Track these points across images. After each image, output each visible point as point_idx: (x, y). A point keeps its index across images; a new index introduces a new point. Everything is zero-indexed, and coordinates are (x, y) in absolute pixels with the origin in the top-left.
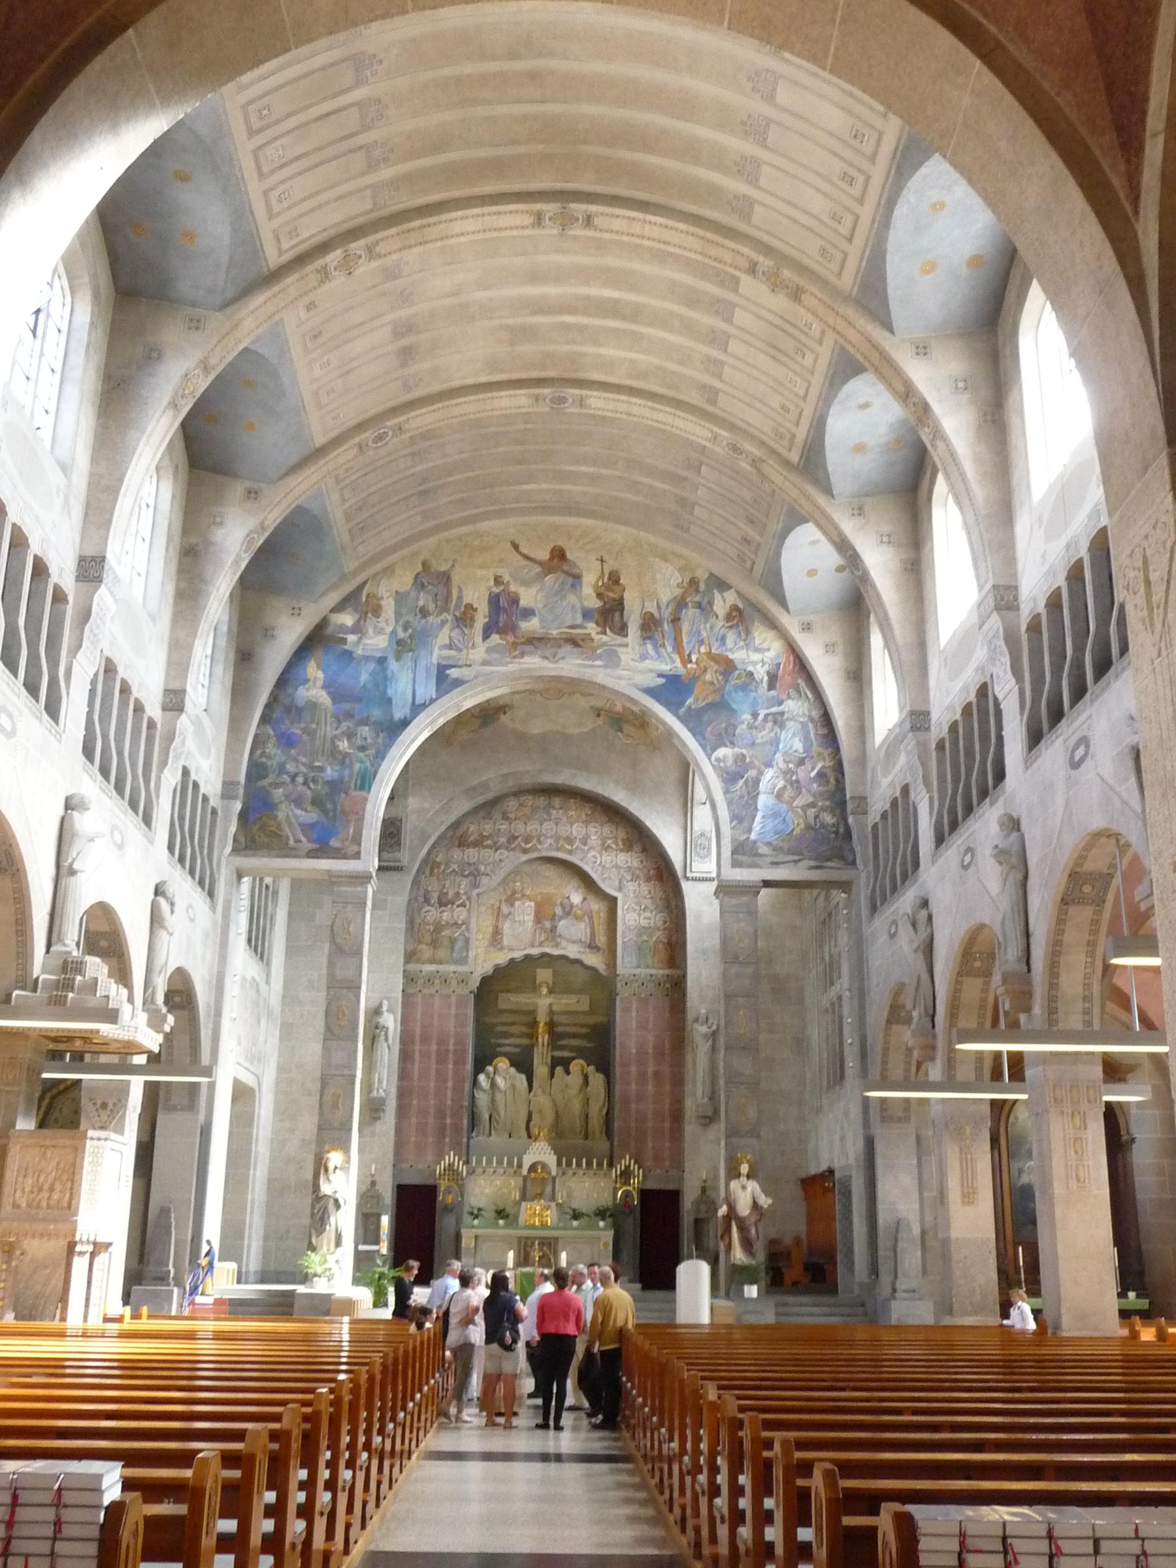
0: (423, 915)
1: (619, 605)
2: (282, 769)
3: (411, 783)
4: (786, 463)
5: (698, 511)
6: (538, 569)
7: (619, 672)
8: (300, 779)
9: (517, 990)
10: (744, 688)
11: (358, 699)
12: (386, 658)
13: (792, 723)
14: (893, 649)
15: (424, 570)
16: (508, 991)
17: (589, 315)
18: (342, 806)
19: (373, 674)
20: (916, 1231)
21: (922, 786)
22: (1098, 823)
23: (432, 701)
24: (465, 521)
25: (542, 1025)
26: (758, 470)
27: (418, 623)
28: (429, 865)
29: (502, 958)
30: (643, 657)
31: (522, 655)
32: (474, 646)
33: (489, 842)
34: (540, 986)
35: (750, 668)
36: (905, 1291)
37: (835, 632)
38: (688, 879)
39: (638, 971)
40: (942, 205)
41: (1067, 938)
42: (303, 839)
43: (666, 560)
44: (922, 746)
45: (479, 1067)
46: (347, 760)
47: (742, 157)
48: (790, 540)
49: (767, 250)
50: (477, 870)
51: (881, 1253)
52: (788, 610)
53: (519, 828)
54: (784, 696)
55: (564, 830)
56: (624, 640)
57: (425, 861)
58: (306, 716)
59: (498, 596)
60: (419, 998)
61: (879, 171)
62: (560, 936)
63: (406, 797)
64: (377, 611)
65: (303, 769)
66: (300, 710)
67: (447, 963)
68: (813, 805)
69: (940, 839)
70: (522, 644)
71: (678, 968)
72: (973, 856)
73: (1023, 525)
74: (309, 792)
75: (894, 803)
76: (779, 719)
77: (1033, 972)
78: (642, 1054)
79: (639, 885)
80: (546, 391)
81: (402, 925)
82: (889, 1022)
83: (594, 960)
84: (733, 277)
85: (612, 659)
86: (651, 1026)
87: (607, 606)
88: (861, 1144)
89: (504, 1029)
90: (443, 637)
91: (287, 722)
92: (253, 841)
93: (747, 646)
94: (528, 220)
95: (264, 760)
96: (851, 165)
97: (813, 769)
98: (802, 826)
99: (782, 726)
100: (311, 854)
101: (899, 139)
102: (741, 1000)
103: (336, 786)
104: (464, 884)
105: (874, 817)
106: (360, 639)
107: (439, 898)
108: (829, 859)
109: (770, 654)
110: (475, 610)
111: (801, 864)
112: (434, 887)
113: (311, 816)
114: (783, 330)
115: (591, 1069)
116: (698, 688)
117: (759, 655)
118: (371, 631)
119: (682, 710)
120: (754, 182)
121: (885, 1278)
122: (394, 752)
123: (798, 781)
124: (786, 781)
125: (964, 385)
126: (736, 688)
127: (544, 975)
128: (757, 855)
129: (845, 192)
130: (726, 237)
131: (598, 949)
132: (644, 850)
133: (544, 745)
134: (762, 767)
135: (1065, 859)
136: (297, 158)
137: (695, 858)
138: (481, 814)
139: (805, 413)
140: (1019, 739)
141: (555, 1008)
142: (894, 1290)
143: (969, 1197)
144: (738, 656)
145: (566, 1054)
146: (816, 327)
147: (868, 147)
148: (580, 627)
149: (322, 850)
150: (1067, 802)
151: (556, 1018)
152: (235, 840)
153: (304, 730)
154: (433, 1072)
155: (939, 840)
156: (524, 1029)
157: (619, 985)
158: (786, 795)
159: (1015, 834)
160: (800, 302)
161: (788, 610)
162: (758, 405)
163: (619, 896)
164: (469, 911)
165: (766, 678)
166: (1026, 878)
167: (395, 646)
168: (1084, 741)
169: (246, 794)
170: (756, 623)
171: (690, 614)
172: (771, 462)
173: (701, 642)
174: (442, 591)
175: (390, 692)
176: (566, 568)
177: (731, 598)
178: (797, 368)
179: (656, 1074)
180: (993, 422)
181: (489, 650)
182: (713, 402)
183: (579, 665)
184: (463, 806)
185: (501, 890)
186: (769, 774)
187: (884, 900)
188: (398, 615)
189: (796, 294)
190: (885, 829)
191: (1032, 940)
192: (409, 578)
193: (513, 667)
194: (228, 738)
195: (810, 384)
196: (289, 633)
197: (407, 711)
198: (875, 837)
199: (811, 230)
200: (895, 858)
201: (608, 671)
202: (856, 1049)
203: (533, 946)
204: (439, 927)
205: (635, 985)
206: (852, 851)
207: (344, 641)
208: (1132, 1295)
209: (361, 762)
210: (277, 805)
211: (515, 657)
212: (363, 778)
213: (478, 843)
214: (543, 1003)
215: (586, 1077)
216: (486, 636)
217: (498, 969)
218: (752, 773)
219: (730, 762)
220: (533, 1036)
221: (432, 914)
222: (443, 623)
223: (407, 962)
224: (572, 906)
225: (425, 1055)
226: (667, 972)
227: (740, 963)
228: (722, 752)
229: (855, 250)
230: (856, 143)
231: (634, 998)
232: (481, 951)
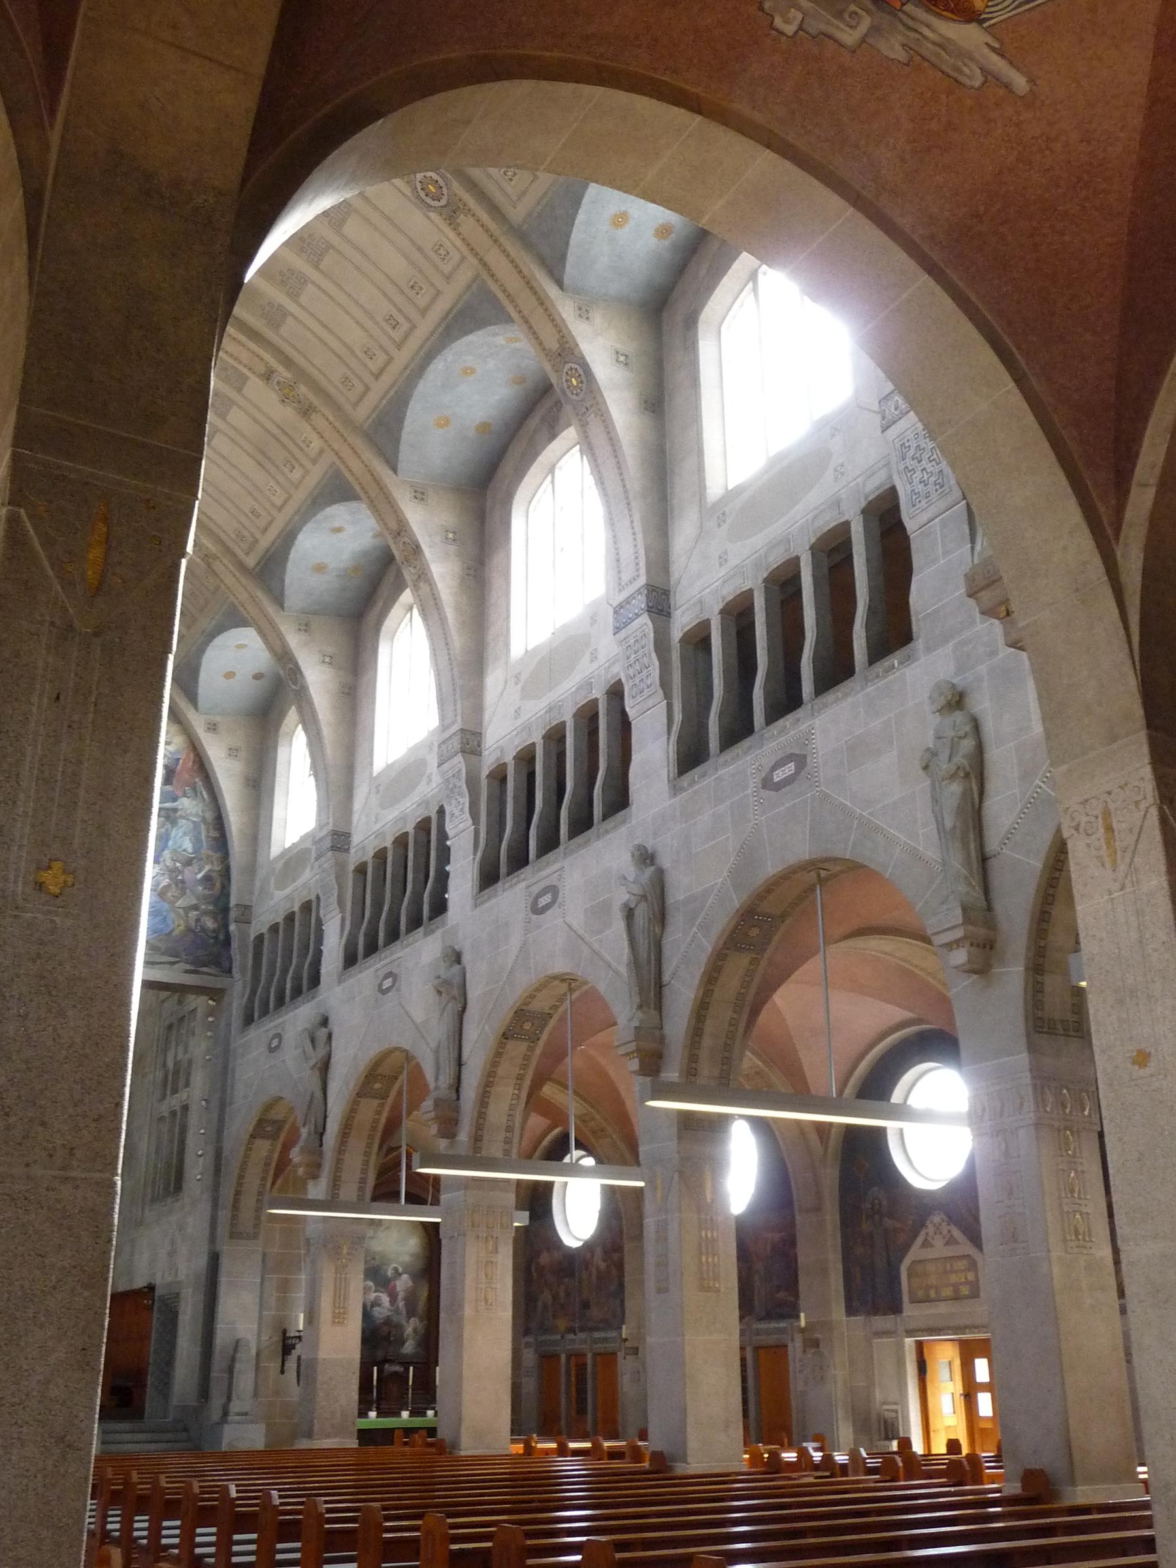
4: (242, 566)
20: (254, 1352)
21: (336, 905)
22: (561, 966)
26: (209, 565)
36: (238, 1414)
40: (473, 371)
41: (501, 1071)
44: (341, 867)
47: (289, 270)
48: (219, 641)
49: (288, 362)
51: (214, 1374)
54: (179, 793)
61: (426, 326)
68: (195, 907)
72: (394, 982)
73: (494, 680)
75: (290, 918)
76: (172, 814)
77: (462, 1101)
82: (253, 1136)
84: (242, 375)
88: (202, 1262)
96: (400, 310)
98: (182, 928)
99: (174, 823)
101: (455, 304)
105: (254, 930)
114: (278, 440)
120: (294, 296)
121: (217, 1402)
124: (171, 879)
125: (454, 537)
129: (386, 333)
130: (250, 338)
135: (512, 999)
140: (469, 876)
142: (226, 1413)
143: (339, 1317)
146: (316, 444)
147: (422, 301)
150: (525, 944)
155: (350, 960)
158: (169, 894)
159: (457, 967)
160: (308, 420)
162: (228, 504)
166: (464, 1008)
168: (553, 890)
172: (226, 561)
178: (281, 479)
180: (475, 576)
187: (265, 1012)
189: (306, 412)
190: (274, 943)
191: (464, 1070)
195: (290, 496)
199: (339, 357)
200: (285, 971)
206: (230, 959)
208: (373, 1414)
229: (378, 389)
230: (412, 294)
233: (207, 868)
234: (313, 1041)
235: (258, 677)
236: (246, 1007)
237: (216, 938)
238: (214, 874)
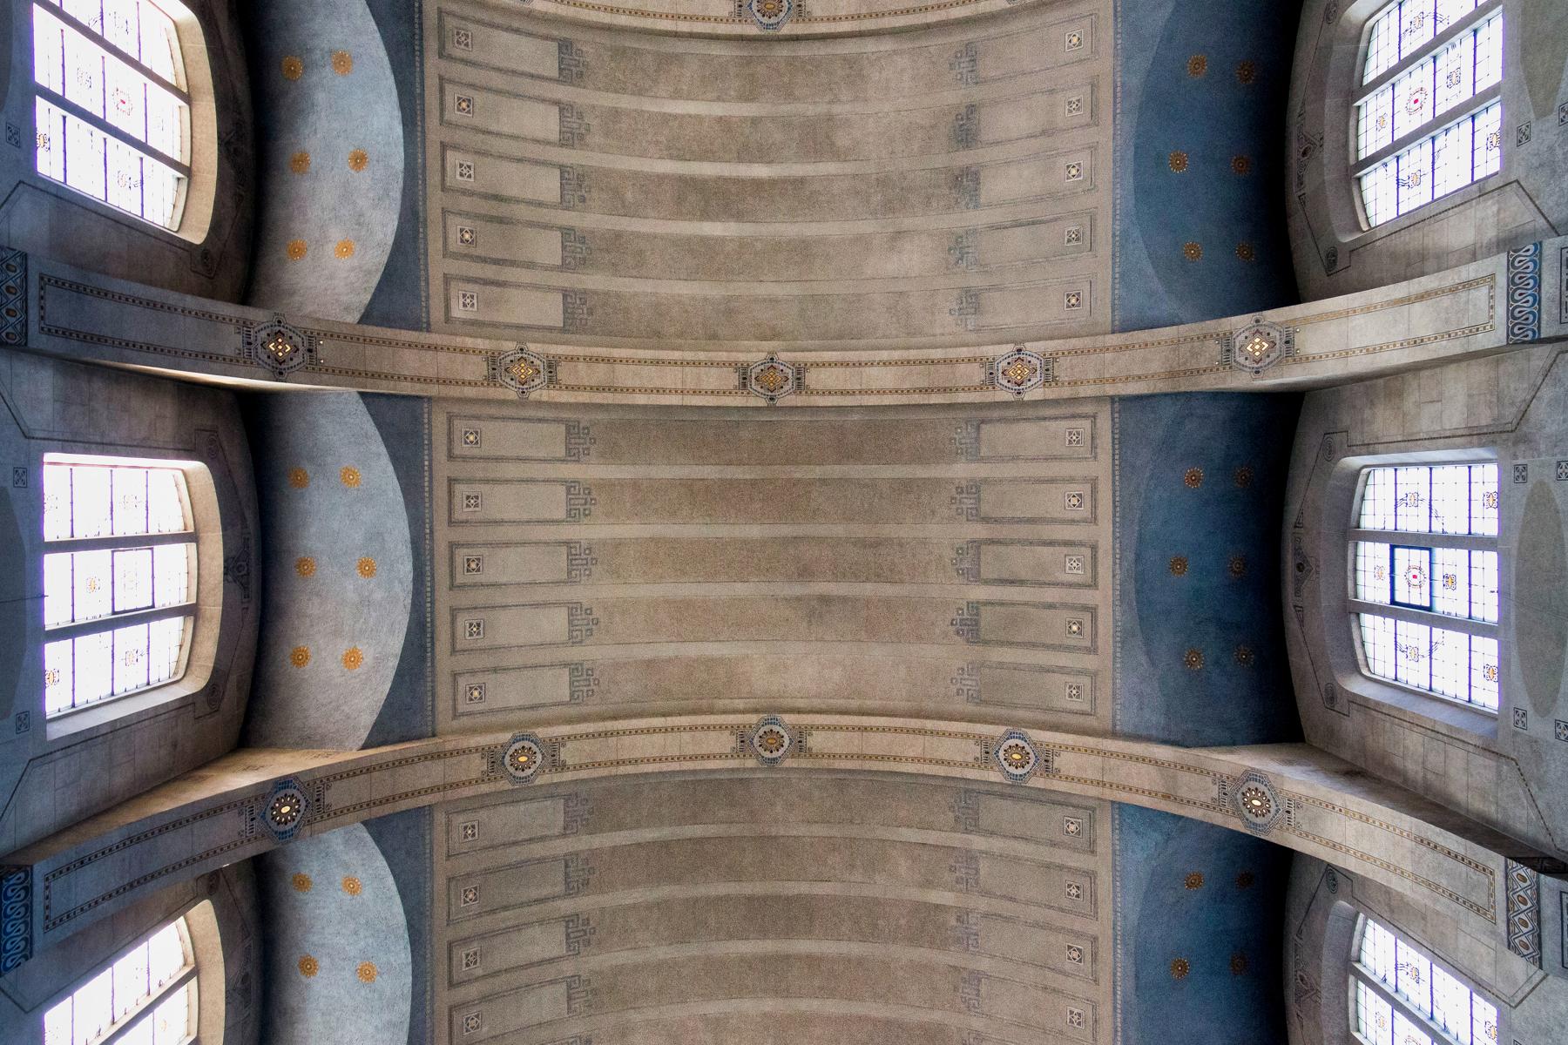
17: (737, 181)
94: (813, 378)
96: (482, 650)
101: (433, 665)
114: (496, 262)
136: (1051, 543)
182: (565, 46)
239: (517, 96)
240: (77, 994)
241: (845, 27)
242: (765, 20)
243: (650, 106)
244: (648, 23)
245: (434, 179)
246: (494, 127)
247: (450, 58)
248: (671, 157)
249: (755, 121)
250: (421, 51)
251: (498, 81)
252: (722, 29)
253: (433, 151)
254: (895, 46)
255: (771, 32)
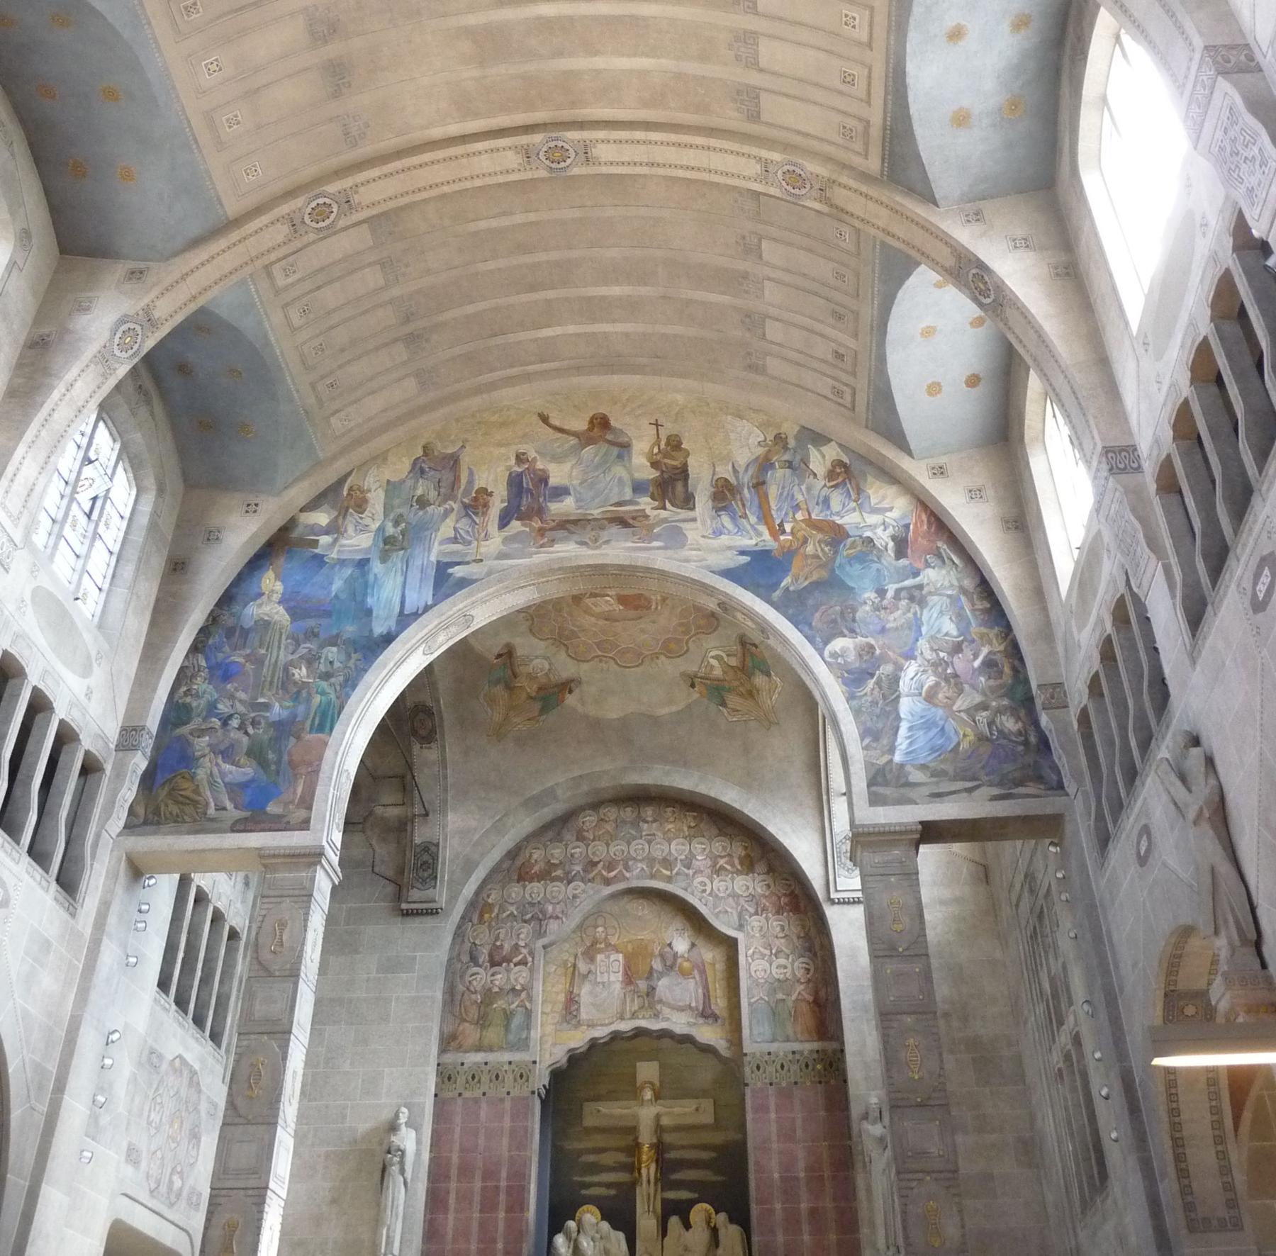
0: (467, 978)
1: (683, 473)
2: (212, 708)
3: (450, 794)
4: (865, 177)
5: (774, 331)
6: (573, 441)
7: (685, 553)
8: (235, 723)
9: (612, 1096)
10: (862, 558)
11: (328, 614)
12: (368, 560)
13: (936, 598)
14: (1065, 392)
15: (425, 454)
16: (597, 1098)
18: (290, 754)
19: (349, 582)
23: (427, 608)
24: (478, 390)
25: (646, 1148)
27: (414, 516)
28: (478, 908)
29: (578, 1039)
30: (718, 533)
31: (553, 542)
32: (486, 537)
33: (559, 872)
34: (642, 1088)
35: (868, 534)
37: (981, 473)
38: (832, 902)
39: (774, 1047)
42: (229, 805)
43: (741, 418)
45: (556, 1225)
46: (304, 693)
50: (543, 912)
52: (910, 453)
53: (599, 851)
55: (659, 850)
56: (691, 514)
57: (472, 904)
58: (254, 638)
59: (520, 475)
60: (458, 1106)
62: (660, 1001)
63: (444, 812)
64: (361, 506)
65: (240, 708)
66: (245, 633)
67: (501, 1048)
68: (983, 706)
69: (1196, 613)
70: (551, 529)
71: (831, 1039)
74: (245, 739)
76: (916, 593)
78: (789, 1183)
79: (767, 919)
80: (537, 138)
81: (438, 993)
83: (709, 1034)
85: (675, 537)
86: (799, 1132)
87: (666, 476)
89: (591, 1158)
90: (447, 529)
91: (227, 649)
92: (157, 812)
93: (861, 507)
95: (188, 700)
97: (976, 656)
98: (971, 737)
99: (922, 603)
100: (240, 826)
102: (909, 1020)
103: (284, 729)
104: (526, 930)
105: (1078, 694)
106: (336, 540)
107: (491, 955)
108: (1020, 783)
109: (895, 514)
110: (491, 494)
111: (976, 793)
112: (483, 937)
113: (244, 771)
115: (722, 1218)
116: (797, 563)
117: (880, 515)
118: (351, 530)
119: (777, 595)
122: (372, 677)
123: (956, 676)
126: (851, 560)
127: (647, 1071)
128: (909, 784)
131: (715, 1017)
132: (771, 870)
133: (622, 734)
134: (901, 660)
137: (840, 871)
138: (550, 834)
139: (875, 75)
141: (665, 1121)
144: (850, 519)
145: (684, 1195)
148: (631, 502)
149: (255, 820)
151: (668, 1138)
152: (131, 812)
153: (248, 658)
154: (475, 1226)
156: (622, 1158)
157: (747, 1070)
158: (940, 696)
161: (910, 453)
163: (740, 936)
164: (531, 970)
165: (891, 544)
167: (381, 545)
169: (157, 748)
170: (870, 479)
171: (778, 478)
173: (797, 508)
174: (447, 476)
175: (370, 601)
176: (609, 437)
177: (832, 452)
179: (813, 1212)
181: (506, 541)
182: (755, 117)
183: (629, 549)
184: (525, 824)
185: (578, 939)
186: (911, 669)
188: (387, 509)
190: (1102, 711)
192: (406, 464)
193: (539, 558)
194: (139, 669)
196: (240, 533)
197: (392, 624)
198: (1088, 737)
200: (1123, 728)
201: (669, 553)
202: (1119, 1100)
203: (622, 1018)
204: (489, 996)
205: (771, 1069)
207: (315, 543)
209: (323, 693)
210: (198, 759)
211: (542, 546)
212: (324, 715)
213: (545, 875)
214: (646, 1114)
215: (714, 1231)
216: (504, 522)
217: (574, 1059)
218: (886, 669)
219: (852, 657)
220: (632, 1168)
221: (480, 977)
222: (447, 513)
223: (443, 1050)
224: (675, 956)
225: (464, 1197)
226: (815, 1045)
227: (900, 955)
228: (838, 644)
231: (771, 1090)
232: (550, 1029)
233: (985, 651)
234: (1183, 778)
235: (973, 381)
236: (1096, 828)
237: (1026, 743)
238: (998, 657)
239: (801, 80)
240: (1143, 299)
241: (480, 146)
242: (560, 144)
243: (667, 63)
244: (673, 137)
245: (881, 19)
246: (822, 55)
247: (860, 119)
248: (645, 19)
249: (559, 53)
250: (885, 129)
251: (819, 95)
252: (601, 134)
253: (879, 44)
254: (427, 132)
255: (554, 135)
